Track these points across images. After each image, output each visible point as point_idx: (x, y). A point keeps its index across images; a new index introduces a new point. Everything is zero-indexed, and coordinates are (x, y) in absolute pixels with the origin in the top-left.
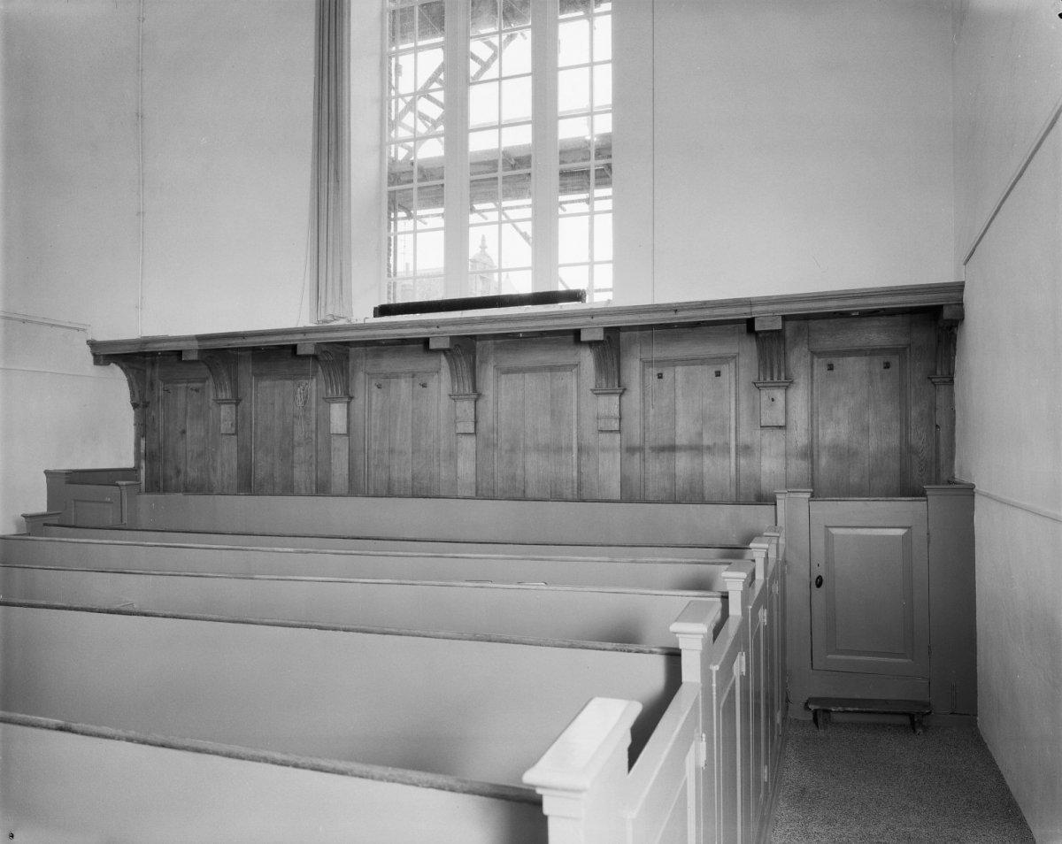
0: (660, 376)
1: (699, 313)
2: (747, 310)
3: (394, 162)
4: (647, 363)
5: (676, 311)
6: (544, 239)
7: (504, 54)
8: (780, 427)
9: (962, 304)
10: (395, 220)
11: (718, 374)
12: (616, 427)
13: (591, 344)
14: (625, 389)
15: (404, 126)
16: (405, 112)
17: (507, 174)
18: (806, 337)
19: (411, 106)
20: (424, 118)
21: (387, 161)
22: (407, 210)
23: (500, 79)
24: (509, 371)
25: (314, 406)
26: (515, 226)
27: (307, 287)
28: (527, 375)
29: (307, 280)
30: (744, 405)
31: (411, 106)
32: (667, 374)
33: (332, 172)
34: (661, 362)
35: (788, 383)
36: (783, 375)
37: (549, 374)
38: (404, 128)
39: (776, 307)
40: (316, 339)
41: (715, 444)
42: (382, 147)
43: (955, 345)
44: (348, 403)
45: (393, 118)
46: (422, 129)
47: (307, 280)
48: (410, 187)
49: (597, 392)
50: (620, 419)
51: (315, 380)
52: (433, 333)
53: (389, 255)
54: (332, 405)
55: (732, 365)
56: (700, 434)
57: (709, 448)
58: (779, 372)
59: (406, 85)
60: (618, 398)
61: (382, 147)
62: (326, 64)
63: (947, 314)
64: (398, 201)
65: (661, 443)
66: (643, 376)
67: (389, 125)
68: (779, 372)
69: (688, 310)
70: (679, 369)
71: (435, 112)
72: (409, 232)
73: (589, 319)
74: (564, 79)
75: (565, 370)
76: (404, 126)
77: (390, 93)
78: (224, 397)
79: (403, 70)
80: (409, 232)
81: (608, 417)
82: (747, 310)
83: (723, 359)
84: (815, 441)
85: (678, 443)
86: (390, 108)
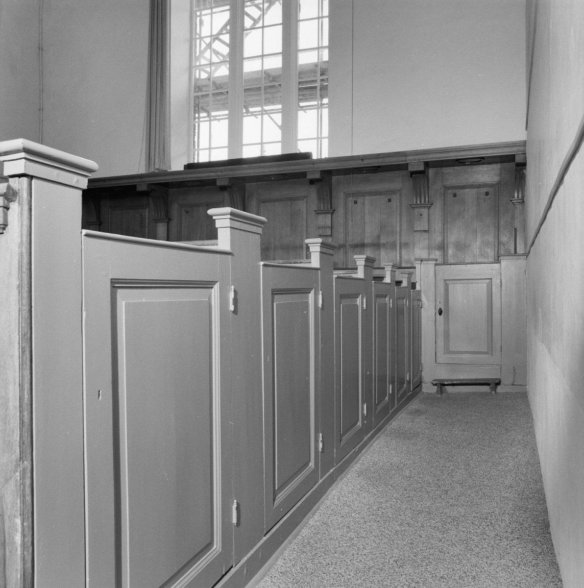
0: (356, 202)
1: (376, 161)
2: (404, 159)
3: (197, 80)
4: (347, 195)
5: (363, 160)
6: (289, 127)
7: (265, 17)
8: (425, 231)
9: (525, 153)
10: (199, 118)
11: (390, 200)
12: (329, 233)
13: (312, 182)
14: (334, 210)
15: (205, 58)
16: (206, 49)
17: (266, 89)
18: (441, 178)
19: (209, 46)
20: (217, 53)
21: (187, 170)
22: (208, 112)
23: (263, 27)
24: (264, 202)
25: (147, 225)
26: (269, 116)
27: (144, 149)
28: (276, 204)
29: (144, 144)
30: (404, 219)
31: (209, 46)
32: (360, 200)
33: (159, 87)
34: (354, 194)
35: (429, 205)
36: (427, 199)
37: (289, 202)
38: (205, 59)
39: (420, 157)
40: (148, 181)
41: (387, 242)
42: (190, 68)
43: (525, 180)
44: (168, 223)
45: (197, 55)
46: (215, 59)
47: (144, 144)
48: (207, 96)
49: (318, 212)
50: (332, 228)
51: (147, 209)
52: (219, 176)
53: (194, 135)
54: (158, 224)
55: (398, 195)
56: (379, 237)
57: (384, 244)
58: (425, 197)
59: (205, 31)
60: (330, 215)
61: (190, 68)
62: (156, 16)
63: (518, 159)
64: (201, 105)
65: (355, 242)
66: (346, 204)
67: (195, 59)
68: (425, 197)
69: (370, 159)
70: (367, 198)
71: (225, 50)
72: (207, 149)
73: (312, 166)
74: (302, 26)
75: (299, 200)
76: (205, 58)
77: (195, 36)
78: (91, 221)
79: (204, 23)
80: (207, 149)
81: (324, 227)
82: (404, 159)
83: (393, 192)
84: (446, 241)
85: (366, 241)
86: (196, 46)
